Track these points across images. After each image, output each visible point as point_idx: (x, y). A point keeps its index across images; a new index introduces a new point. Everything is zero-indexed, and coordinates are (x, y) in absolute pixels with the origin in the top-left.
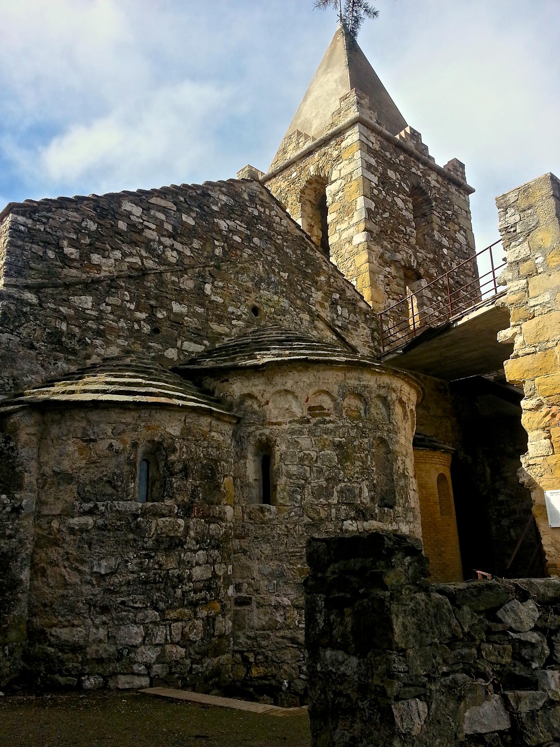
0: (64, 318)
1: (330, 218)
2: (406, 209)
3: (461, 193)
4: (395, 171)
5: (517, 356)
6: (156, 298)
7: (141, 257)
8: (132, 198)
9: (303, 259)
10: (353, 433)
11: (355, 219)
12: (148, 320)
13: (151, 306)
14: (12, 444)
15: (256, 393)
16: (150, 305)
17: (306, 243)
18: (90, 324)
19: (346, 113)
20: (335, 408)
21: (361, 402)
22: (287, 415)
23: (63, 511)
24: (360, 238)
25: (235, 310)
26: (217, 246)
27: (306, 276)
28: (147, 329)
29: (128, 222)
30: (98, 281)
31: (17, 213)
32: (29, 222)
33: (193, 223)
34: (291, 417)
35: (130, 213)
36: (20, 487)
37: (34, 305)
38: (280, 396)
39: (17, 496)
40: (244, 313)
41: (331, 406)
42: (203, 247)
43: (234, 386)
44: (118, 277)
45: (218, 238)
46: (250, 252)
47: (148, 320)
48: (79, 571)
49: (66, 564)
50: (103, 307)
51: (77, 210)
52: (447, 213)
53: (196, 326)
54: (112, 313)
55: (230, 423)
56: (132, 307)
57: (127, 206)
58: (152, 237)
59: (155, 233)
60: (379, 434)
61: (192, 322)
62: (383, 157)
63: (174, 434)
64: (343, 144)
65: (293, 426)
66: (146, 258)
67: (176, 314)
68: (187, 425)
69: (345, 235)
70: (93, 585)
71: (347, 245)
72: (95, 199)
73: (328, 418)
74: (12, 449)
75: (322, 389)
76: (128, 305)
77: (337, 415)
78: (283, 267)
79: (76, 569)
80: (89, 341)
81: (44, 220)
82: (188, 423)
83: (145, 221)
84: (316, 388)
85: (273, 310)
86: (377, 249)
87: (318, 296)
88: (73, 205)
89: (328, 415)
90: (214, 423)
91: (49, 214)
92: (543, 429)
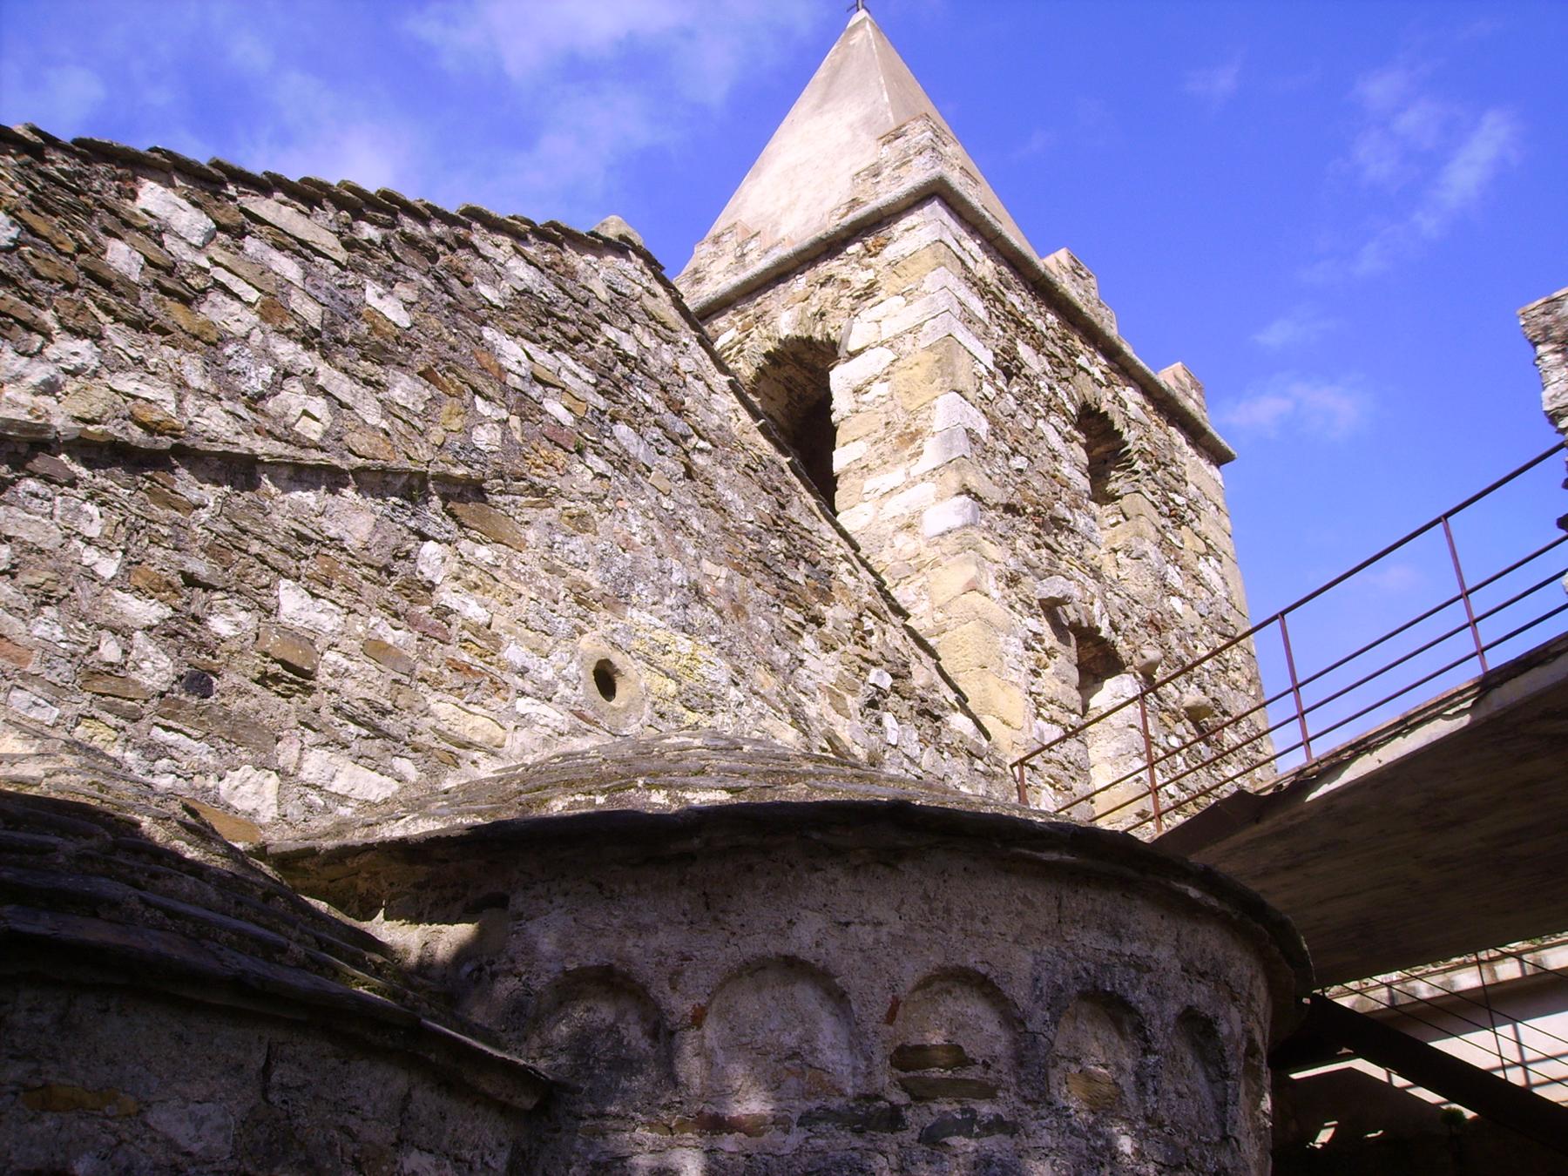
1: (841, 459)
4: (1038, 348)
7: (182, 385)
12: (168, 634)
13: (191, 580)
15: (645, 968)
16: (184, 574)
19: (896, 173)
20: (1020, 1061)
21: (1122, 1034)
22: (792, 1082)
25: (533, 662)
26: (482, 420)
29: (153, 255)
33: (404, 320)
34: (806, 1095)
38: (759, 989)
40: (566, 680)
41: (998, 1048)
43: (532, 928)
45: (490, 392)
47: (168, 634)
52: (1173, 500)
53: (371, 695)
55: (504, 1109)
56: (108, 567)
63: (196, 1147)
64: (890, 253)
65: (821, 1142)
66: (200, 393)
67: (291, 634)
68: (274, 1097)
75: (958, 961)
76: (90, 556)
77: (1027, 1092)
82: (284, 1087)
83: (217, 264)
84: (936, 959)
87: (822, 668)
90: (427, 1101)
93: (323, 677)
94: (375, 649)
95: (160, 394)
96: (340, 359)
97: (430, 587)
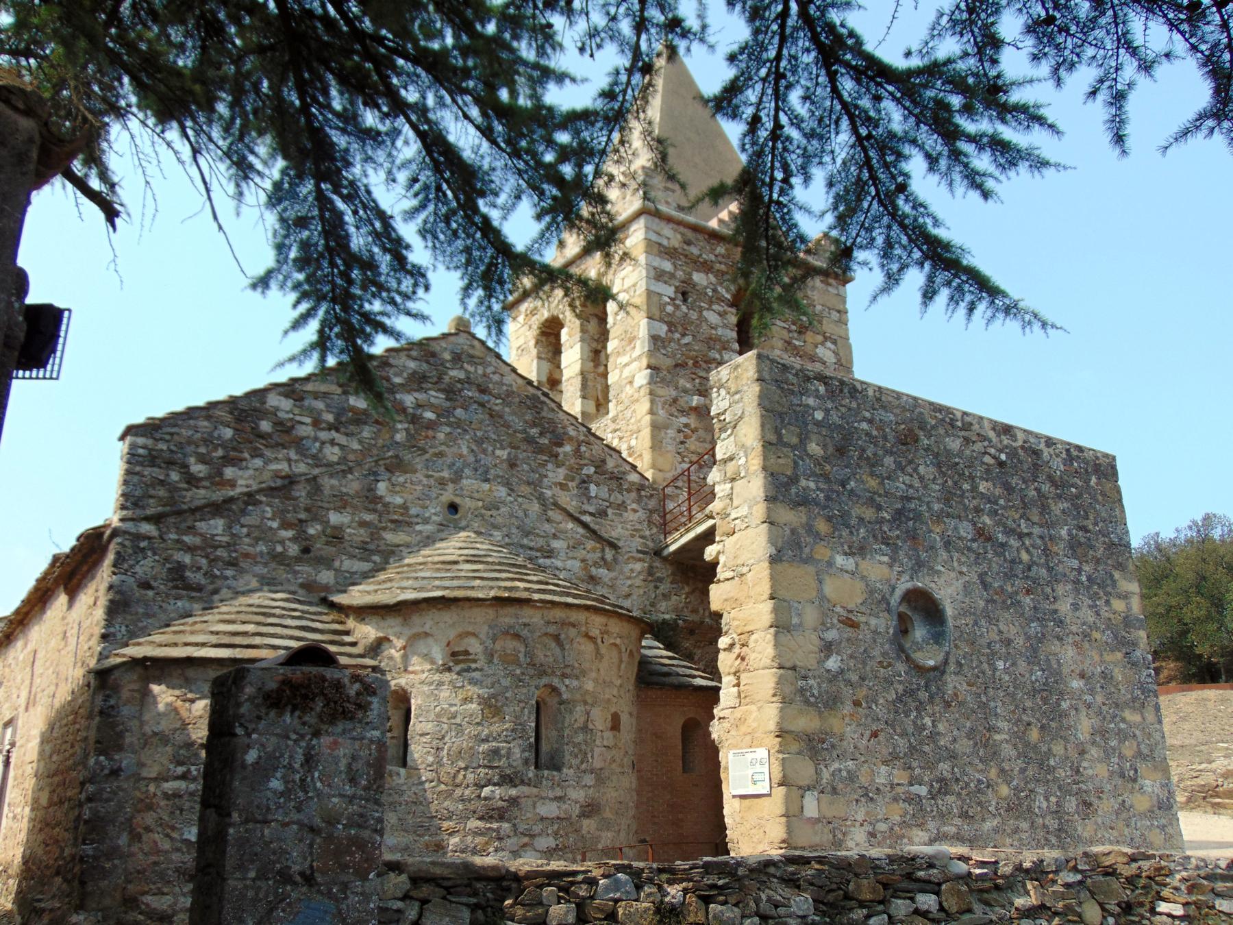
0: (190, 549)
1: (611, 346)
2: (725, 326)
3: (830, 285)
5: (719, 581)
6: (307, 510)
7: (289, 460)
8: (281, 389)
9: (534, 425)
10: (506, 682)
11: (637, 352)
13: (301, 521)
14: (112, 702)
17: (544, 403)
18: (220, 552)
23: (159, 774)
24: (642, 378)
26: (397, 431)
27: (540, 450)
28: (293, 549)
30: (231, 500)
31: (136, 435)
32: (150, 442)
35: (277, 409)
36: (120, 748)
37: (154, 538)
39: (117, 757)
42: (377, 435)
44: (260, 491)
46: (448, 429)
48: (172, 839)
49: (159, 829)
50: (236, 529)
51: (208, 418)
54: (248, 535)
56: (275, 525)
57: (273, 400)
58: (305, 434)
59: (310, 428)
60: (545, 680)
61: (354, 534)
62: (686, 256)
66: (296, 461)
67: (335, 528)
69: (627, 372)
70: (183, 853)
71: (628, 386)
72: (232, 402)
73: (473, 666)
74: (112, 707)
76: (270, 523)
78: (501, 442)
79: (167, 836)
80: (218, 573)
81: (168, 437)
84: (460, 630)
85: (480, 504)
86: (668, 393)
88: (204, 413)
89: (475, 661)
91: (173, 430)
92: (735, 674)
93: (347, 538)
94: (363, 524)
95: (283, 467)
96: (342, 430)
97: (381, 498)
